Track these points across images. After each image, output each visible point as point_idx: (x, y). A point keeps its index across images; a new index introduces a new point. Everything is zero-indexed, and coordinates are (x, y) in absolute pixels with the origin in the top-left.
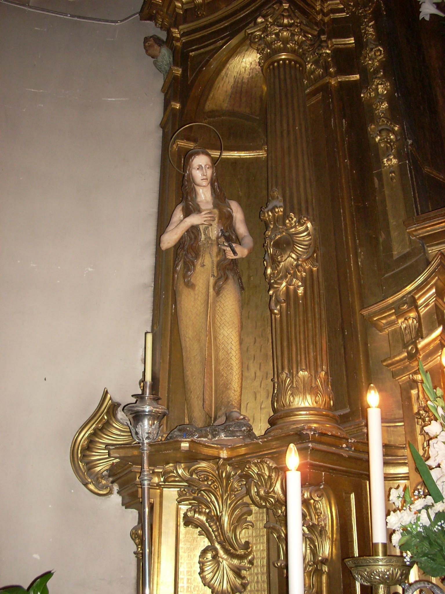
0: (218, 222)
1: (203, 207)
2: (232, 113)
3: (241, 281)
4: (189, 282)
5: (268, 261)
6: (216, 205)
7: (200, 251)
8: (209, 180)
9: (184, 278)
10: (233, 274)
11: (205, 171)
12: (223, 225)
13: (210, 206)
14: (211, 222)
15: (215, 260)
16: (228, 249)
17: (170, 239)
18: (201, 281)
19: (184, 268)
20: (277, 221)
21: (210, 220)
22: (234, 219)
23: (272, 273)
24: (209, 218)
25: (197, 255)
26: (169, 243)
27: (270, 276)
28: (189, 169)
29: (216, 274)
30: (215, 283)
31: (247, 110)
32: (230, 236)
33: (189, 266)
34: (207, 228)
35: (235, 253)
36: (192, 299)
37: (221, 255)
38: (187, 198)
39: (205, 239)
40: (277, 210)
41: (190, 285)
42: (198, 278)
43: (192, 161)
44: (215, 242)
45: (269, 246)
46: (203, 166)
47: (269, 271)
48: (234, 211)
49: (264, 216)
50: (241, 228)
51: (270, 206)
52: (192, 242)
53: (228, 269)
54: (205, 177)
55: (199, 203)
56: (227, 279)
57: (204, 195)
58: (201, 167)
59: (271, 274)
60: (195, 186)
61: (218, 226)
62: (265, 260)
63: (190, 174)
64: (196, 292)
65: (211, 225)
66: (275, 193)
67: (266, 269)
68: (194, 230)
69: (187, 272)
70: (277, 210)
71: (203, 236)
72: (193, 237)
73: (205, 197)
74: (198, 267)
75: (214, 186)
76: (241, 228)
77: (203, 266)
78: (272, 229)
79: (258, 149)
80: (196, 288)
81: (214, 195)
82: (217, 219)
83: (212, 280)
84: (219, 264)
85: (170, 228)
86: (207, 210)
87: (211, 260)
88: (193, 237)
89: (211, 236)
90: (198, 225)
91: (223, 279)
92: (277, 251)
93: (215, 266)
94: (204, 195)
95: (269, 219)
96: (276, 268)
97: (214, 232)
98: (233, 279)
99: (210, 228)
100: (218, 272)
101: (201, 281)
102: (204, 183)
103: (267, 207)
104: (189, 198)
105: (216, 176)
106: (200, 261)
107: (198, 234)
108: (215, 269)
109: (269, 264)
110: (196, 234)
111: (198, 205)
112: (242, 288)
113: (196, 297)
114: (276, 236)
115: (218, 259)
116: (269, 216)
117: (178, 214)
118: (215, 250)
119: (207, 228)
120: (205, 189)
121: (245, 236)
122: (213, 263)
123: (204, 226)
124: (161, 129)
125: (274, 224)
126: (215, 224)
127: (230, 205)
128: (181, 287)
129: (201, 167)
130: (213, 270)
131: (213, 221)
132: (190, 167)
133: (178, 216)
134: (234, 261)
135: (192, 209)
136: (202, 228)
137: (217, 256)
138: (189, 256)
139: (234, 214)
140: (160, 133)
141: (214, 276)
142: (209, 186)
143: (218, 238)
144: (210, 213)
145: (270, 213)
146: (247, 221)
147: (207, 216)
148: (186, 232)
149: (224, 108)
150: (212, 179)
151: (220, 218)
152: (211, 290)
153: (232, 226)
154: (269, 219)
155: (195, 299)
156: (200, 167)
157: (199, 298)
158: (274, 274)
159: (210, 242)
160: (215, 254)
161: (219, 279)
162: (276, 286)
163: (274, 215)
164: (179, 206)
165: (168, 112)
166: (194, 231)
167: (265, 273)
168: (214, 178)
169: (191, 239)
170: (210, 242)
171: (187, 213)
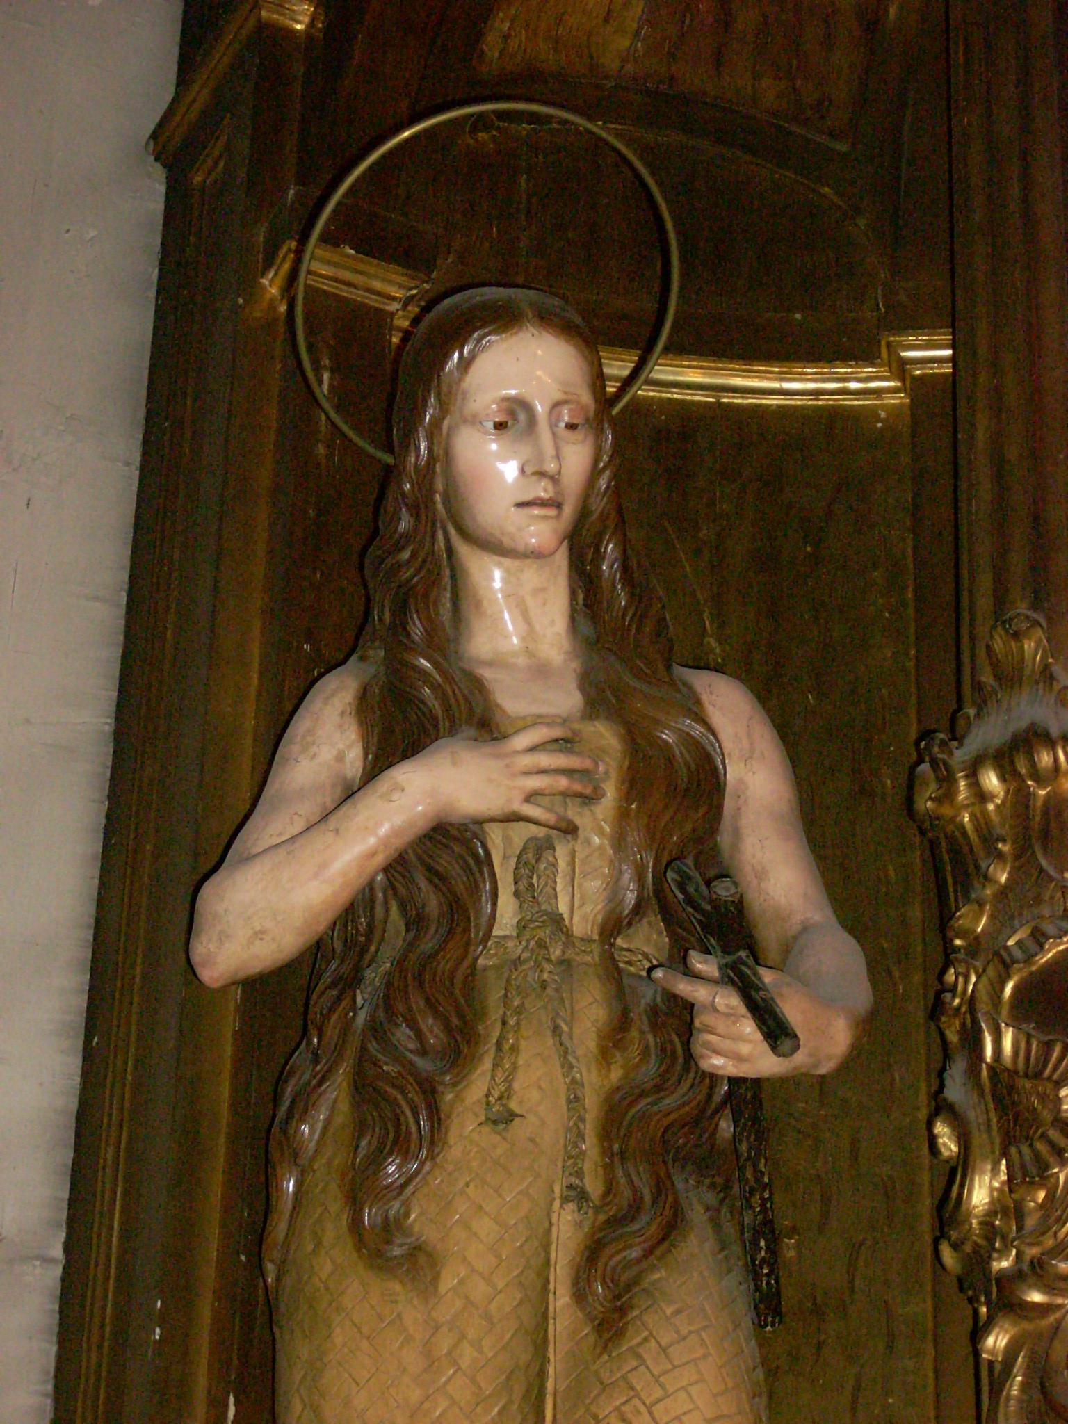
0: (623, 815)
1: (512, 699)
2: (659, 104)
3: (773, 1251)
4: (390, 1228)
5: (974, 1115)
6: (601, 697)
7: (482, 1014)
8: (568, 510)
9: (354, 1202)
10: (711, 1198)
11: (549, 450)
12: (654, 837)
13: (566, 699)
14: (574, 813)
15: (596, 1083)
16: (729, 1000)
17: (266, 904)
18: (485, 1227)
19: (361, 1128)
20: (1046, 836)
21: (565, 794)
22: (728, 804)
23: (1008, 1206)
24: (563, 782)
25: (461, 1045)
26: (259, 934)
27: (987, 1224)
28: (437, 423)
29: (594, 1186)
30: (593, 1252)
31: (770, 91)
32: (701, 910)
33: (399, 1118)
34: (541, 848)
35: (776, 1032)
36: (412, 1359)
37: (634, 1052)
38: (400, 626)
39: (522, 926)
40: (1045, 759)
41: (392, 1252)
42: (462, 1206)
43: (465, 364)
44: (593, 956)
45: (983, 1006)
46: (540, 409)
47: (980, 1195)
48: (728, 745)
49: (948, 795)
50: (775, 871)
51: (988, 732)
52: (427, 945)
53: (686, 1156)
54: (542, 490)
55: (486, 674)
56: (673, 1226)
57: (517, 617)
58: (516, 422)
59: (992, 1213)
60: (464, 550)
61: (619, 841)
62: (940, 1107)
63: (442, 457)
64: (444, 1313)
65: (570, 830)
66: (1029, 646)
67: (956, 1173)
68: (444, 858)
69: (376, 1161)
70: (1045, 759)
71: (507, 913)
72: (433, 903)
73: (530, 634)
74: (466, 1128)
75: (599, 556)
76: (775, 871)
77: (502, 1119)
78: (1003, 892)
79: (845, 356)
80: (448, 1282)
81: (586, 628)
82: (611, 792)
83: (568, 1230)
84: (617, 1116)
85: (269, 828)
86: (537, 721)
87: (561, 1083)
88: (433, 903)
89: (563, 908)
90: (480, 822)
91: (648, 1224)
92: (1048, 1046)
93: (590, 1130)
94: (517, 617)
95: (982, 823)
96: (1043, 1167)
97: (588, 882)
98: (716, 1223)
99: (561, 852)
100: (608, 1169)
101: (485, 1227)
102: (539, 531)
103: (956, 736)
104: (417, 630)
105: (616, 492)
106: (479, 1084)
107: (475, 888)
108: (590, 1146)
109: (979, 1139)
110: (460, 887)
111: (478, 685)
112: (768, 1306)
113: (444, 1343)
114: (1039, 938)
115: (616, 1074)
116: (982, 796)
117: (328, 735)
118: (591, 1011)
119: (541, 848)
120: (531, 576)
121: (805, 929)
122: (575, 1100)
123: (521, 834)
124: (159, 173)
125: (1023, 853)
126: (597, 824)
127: (698, 702)
128: (325, 1268)
129: (516, 422)
130: (573, 1158)
131: (589, 799)
132: (444, 409)
133: (326, 754)
134: (746, 1095)
135: (435, 705)
136: (502, 847)
137: (605, 1057)
138: (402, 1035)
139: (734, 772)
140: (150, 193)
141: (581, 1196)
142: (561, 560)
143: (613, 926)
144: (565, 744)
145: (992, 781)
146: (824, 826)
147: (545, 760)
148: (386, 870)
149: (611, 63)
150: (583, 514)
151: (636, 784)
152: (561, 1298)
153: (715, 852)
154: (982, 823)
155: (431, 1363)
156: (513, 419)
157: (467, 1355)
158: (1019, 1213)
159: (556, 953)
160: (592, 1044)
161: (616, 1222)
162: (1036, 1297)
163: (1020, 799)
164: (331, 682)
165: (221, 56)
166: (446, 863)
167: (948, 1208)
168: (598, 505)
169: (416, 922)
170: (556, 953)
171: (398, 732)
